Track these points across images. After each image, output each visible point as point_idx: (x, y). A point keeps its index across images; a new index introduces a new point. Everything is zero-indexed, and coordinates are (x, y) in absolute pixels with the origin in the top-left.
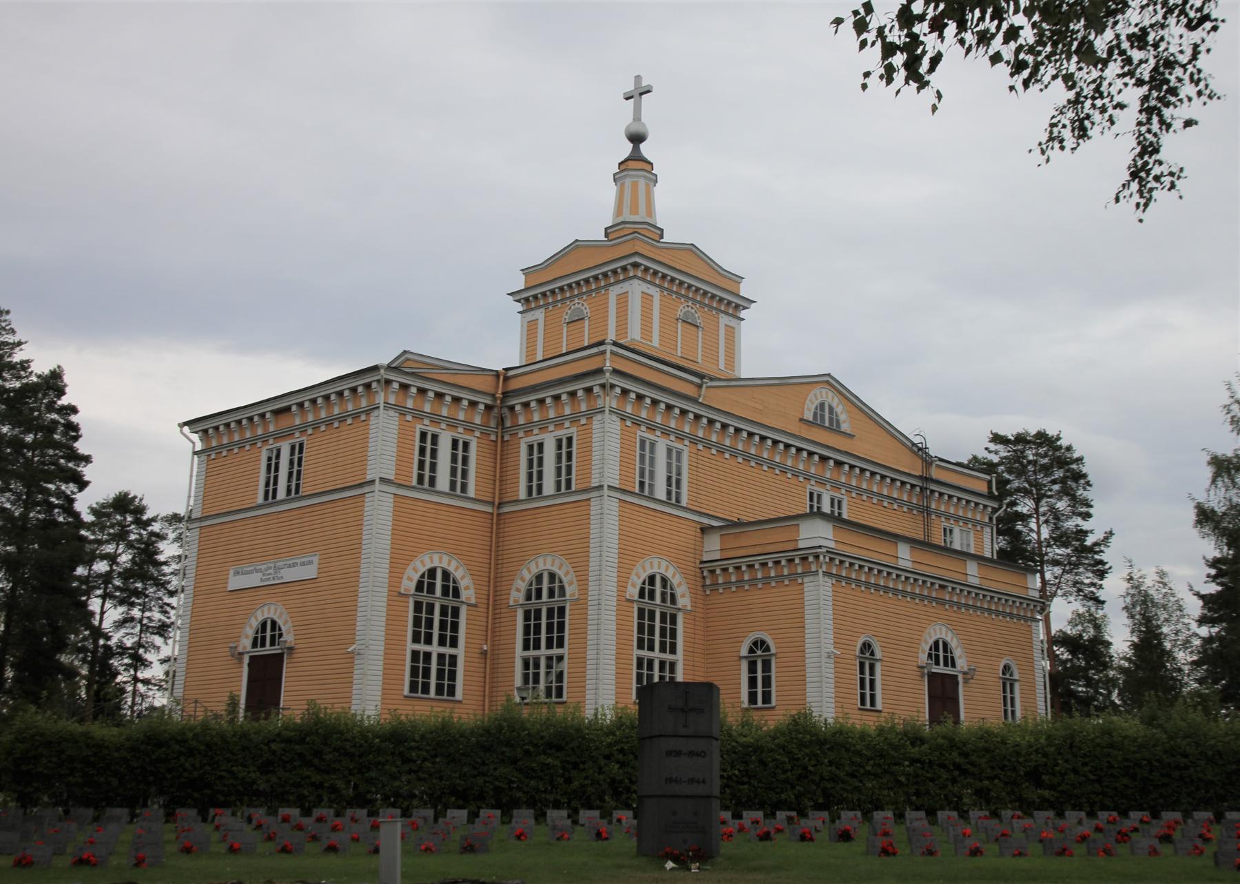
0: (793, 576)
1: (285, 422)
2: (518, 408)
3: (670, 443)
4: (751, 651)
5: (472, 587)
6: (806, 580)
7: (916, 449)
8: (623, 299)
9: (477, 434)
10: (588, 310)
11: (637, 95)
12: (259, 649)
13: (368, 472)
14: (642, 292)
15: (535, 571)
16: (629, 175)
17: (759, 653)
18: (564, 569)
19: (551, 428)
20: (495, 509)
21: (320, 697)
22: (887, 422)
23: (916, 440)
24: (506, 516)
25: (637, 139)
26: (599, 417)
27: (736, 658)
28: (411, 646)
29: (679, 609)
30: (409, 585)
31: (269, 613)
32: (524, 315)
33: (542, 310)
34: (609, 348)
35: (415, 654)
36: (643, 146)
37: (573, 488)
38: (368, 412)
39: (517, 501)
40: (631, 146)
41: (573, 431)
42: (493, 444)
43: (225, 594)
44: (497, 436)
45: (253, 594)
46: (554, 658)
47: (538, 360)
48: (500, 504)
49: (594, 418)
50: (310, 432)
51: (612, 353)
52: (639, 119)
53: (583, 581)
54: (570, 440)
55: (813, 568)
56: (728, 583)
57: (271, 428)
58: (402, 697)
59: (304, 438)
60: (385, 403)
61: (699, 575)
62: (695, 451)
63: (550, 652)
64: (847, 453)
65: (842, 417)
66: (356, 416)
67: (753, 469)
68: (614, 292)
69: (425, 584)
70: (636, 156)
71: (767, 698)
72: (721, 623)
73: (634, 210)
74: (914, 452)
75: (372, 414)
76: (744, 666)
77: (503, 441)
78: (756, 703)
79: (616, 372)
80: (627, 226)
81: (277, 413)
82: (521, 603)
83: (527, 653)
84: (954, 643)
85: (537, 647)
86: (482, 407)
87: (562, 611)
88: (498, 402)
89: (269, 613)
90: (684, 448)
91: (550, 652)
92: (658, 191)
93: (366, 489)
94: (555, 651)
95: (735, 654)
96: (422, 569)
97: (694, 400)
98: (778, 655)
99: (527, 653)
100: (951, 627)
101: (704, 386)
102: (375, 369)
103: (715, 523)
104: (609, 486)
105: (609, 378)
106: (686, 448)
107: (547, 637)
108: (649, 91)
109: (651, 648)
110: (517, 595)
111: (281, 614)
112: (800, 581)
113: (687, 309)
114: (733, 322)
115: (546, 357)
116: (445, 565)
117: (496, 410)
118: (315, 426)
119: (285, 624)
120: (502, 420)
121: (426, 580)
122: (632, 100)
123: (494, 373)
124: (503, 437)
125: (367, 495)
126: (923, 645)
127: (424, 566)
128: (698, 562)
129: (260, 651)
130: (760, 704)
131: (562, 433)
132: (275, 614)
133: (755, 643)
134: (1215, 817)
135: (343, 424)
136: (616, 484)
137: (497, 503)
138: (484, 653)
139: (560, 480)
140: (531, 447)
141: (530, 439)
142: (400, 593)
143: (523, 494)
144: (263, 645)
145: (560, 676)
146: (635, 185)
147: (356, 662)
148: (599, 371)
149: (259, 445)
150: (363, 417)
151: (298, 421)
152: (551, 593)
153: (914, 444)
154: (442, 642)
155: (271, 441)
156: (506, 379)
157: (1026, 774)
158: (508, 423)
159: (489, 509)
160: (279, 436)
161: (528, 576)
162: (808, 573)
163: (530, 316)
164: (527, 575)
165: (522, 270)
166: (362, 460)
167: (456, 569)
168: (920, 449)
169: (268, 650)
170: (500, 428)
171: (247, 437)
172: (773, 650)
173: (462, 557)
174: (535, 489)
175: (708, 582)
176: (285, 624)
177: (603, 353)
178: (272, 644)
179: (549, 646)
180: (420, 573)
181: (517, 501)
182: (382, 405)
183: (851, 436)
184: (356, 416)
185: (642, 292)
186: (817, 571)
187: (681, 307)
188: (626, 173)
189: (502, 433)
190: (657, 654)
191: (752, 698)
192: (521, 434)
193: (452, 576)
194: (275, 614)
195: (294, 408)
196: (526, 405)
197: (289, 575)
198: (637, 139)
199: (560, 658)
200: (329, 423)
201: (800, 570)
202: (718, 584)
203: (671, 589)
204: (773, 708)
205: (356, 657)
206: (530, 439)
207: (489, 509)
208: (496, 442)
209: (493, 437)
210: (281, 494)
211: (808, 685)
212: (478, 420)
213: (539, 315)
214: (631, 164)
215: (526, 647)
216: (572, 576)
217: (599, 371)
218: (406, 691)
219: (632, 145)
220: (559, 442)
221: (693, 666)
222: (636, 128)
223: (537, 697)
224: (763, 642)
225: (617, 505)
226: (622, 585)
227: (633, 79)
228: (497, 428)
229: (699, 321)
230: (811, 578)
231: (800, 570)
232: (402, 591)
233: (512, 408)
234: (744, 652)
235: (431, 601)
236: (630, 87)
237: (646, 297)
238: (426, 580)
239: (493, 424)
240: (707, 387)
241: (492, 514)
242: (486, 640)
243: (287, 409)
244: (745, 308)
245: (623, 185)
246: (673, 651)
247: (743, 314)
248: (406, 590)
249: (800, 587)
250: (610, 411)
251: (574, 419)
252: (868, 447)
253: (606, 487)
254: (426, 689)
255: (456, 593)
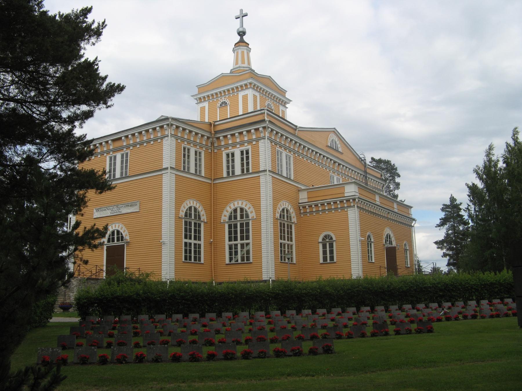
0: (343, 208)
1: (118, 144)
2: (221, 138)
3: (287, 153)
4: (323, 239)
5: (205, 215)
6: (348, 209)
7: (361, 160)
8: (245, 98)
9: (204, 149)
10: (229, 102)
11: (241, 17)
12: (111, 243)
13: (163, 164)
14: (254, 95)
15: (233, 207)
16: (240, 48)
17: (327, 240)
18: (248, 206)
19: (238, 146)
20: (212, 182)
21: (224, 268)
22: (353, 149)
23: (361, 156)
24: (217, 185)
25: (242, 34)
26: (262, 141)
27: (317, 243)
28: (250, 241)
29: (293, 223)
30: (182, 214)
31: (115, 227)
32: (198, 105)
33: (207, 102)
34: (266, 111)
35: (186, 243)
36: (244, 37)
37: (251, 171)
38: (162, 139)
39: (223, 178)
40: (239, 37)
41: (249, 147)
42: (210, 154)
43: (92, 220)
44: (211, 151)
45: (108, 219)
46: (245, 245)
47: (249, 111)
48: (214, 179)
49: (260, 142)
50: (131, 148)
51: (267, 114)
52: (242, 26)
53: (258, 211)
54: (247, 153)
55: (352, 205)
56: (311, 212)
57: (111, 147)
58: (182, 262)
59: (129, 151)
60: (171, 134)
61: (298, 209)
62: (295, 157)
63: (242, 242)
64: (343, 160)
65: (339, 146)
66: (155, 140)
67: (313, 166)
68: (241, 94)
69: (188, 214)
70: (242, 41)
71: (332, 258)
72: (315, 228)
73: (243, 62)
74: (360, 161)
75: (164, 139)
76: (321, 246)
77: (214, 153)
78: (327, 261)
79: (270, 121)
80: (241, 69)
81: (113, 141)
82: (227, 221)
83: (231, 243)
84: (392, 235)
85: (236, 239)
86: (206, 137)
87: (248, 224)
88: (213, 135)
89: (115, 227)
90: (291, 155)
91: (242, 242)
92: (251, 54)
93: (163, 172)
94: (245, 241)
95: (317, 241)
96: (187, 207)
97: (294, 135)
98: (337, 241)
99: (231, 243)
100: (391, 229)
101: (297, 130)
102: (167, 119)
103: (303, 188)
104: (269, 170)
105: (267, 124)
106: (291, 155)
107: (240, 236)
108: (246, 15)
109: (190, 238)
110: (225, 217)
111: (122, 228)
112: (346, 210)
113: (268, 102)
114: (284, 109)
115: (221, 119)
116: (195, 205)
117: (211, 139)
118: (134, 145)
119: (124, 232)
120: (212, 143)
121: (188, 212)
122: (239, 19)
123: (209, 123)
124: (214, 151)
125: (163, 175)
126: (384, 236)
127: (187, 205)
128: (298, 203)
129: (111, 244)
130: (328, 261)
131: (244, 148)
132: (119, 228)
133: (325, 236)
134: (501, 300)
135: (148, 144)
136: (270, 169)
137: (213, 179)
138: (211, 243)
139: (229, 171)
140: (228, 155)
141: (227, 151)
142: (179, 217)
143: (225, 175)
144: (113, 241)
145: (248, 252)
146: (243, 53)
147: (163, 247)
148: (263, 121)
149: (105, 155)
150: (159, 141)
151: (125, 144)
152: (242, 217)
153: (360, 158)
154: (195, 239)
155: (111, 153)
156: (214, 126)
157: (76, 261)
158: (216, 145)
159: (209, 181)
160: (116, 150)
161: (230, 210)
162: (350, 207)
163: (201, 105)
164: (229, 209)
165: (197, 86)
166: (161, 159)
167: (199, 207)
168: (362, 160)
169: (116, 243)
170: (213, 147)
171: (111, 148)
172: (334, 239)
173: (201, 202)
174: (231, 173)
175: (302, 212)
176: (124, 232)
177: (264, 113)
178: (118, 240)
179: (242, 239)
180: (186, 209)
181: (223, 178)
182: (169, 135)
183: (342, 153)
184: (155, 140)
185: (254, 95)
186: (354, 206)
187: (267, 102)
188: (239, 47)
189: (214, 149)
190: (193, 241)
191: (325, 259)
192: (223, 149)
193: (197, 210)
194: (119, 228)
195: (123, 138)
196: (225, 137)
197: (125, 210)
198: (242, 34)
199: (248, 244)
200: (141, 144)
201: (346, 205)
202: (319, 211)
203: (290, 215)
204: (335, 263)
205: (163, 245)
206: (227, 151)
207: (209, 181)
208: (211, 153)
209: (210, 151)
210: (238, 171)
211: (351, 253)
212: (204, 143)
213: (206, 104)
214: (241, 44)
215: (230, 240)
216: (252, 209)
217: (263, 121)
218: (183, 260)
219: (240, 37)
220: (242, 152)
221: (298, 247)
222: (241, 30)
223: (237, 261)
224: (329, 236)
225: (271, 178)
226: (274, 214)
227: (239, 11)
228: (211, 147)
229: (273, 108)
230: (352, 209)
231: (346, 205)
232: (180, 217)
233: (218, 138)
234: (320, 240)
235: (190, 220)
236: (238, 14)
237: (255, 97)
238: (188, 212)
239: (209, 145)
240: (298, 130)
241: (211, 184)
242: (211, 238)
243: (120, 139)
244: (288, 103)
245: (237, 53)
246: (291, 241)
247: (287, 106)
248: (181, 216)
249: (346, 212)
250: (268, 138)
251: (250, 142)
252: (347, 157)
253: (268, 171)
254: (190, 259)
255: (247, 216)
